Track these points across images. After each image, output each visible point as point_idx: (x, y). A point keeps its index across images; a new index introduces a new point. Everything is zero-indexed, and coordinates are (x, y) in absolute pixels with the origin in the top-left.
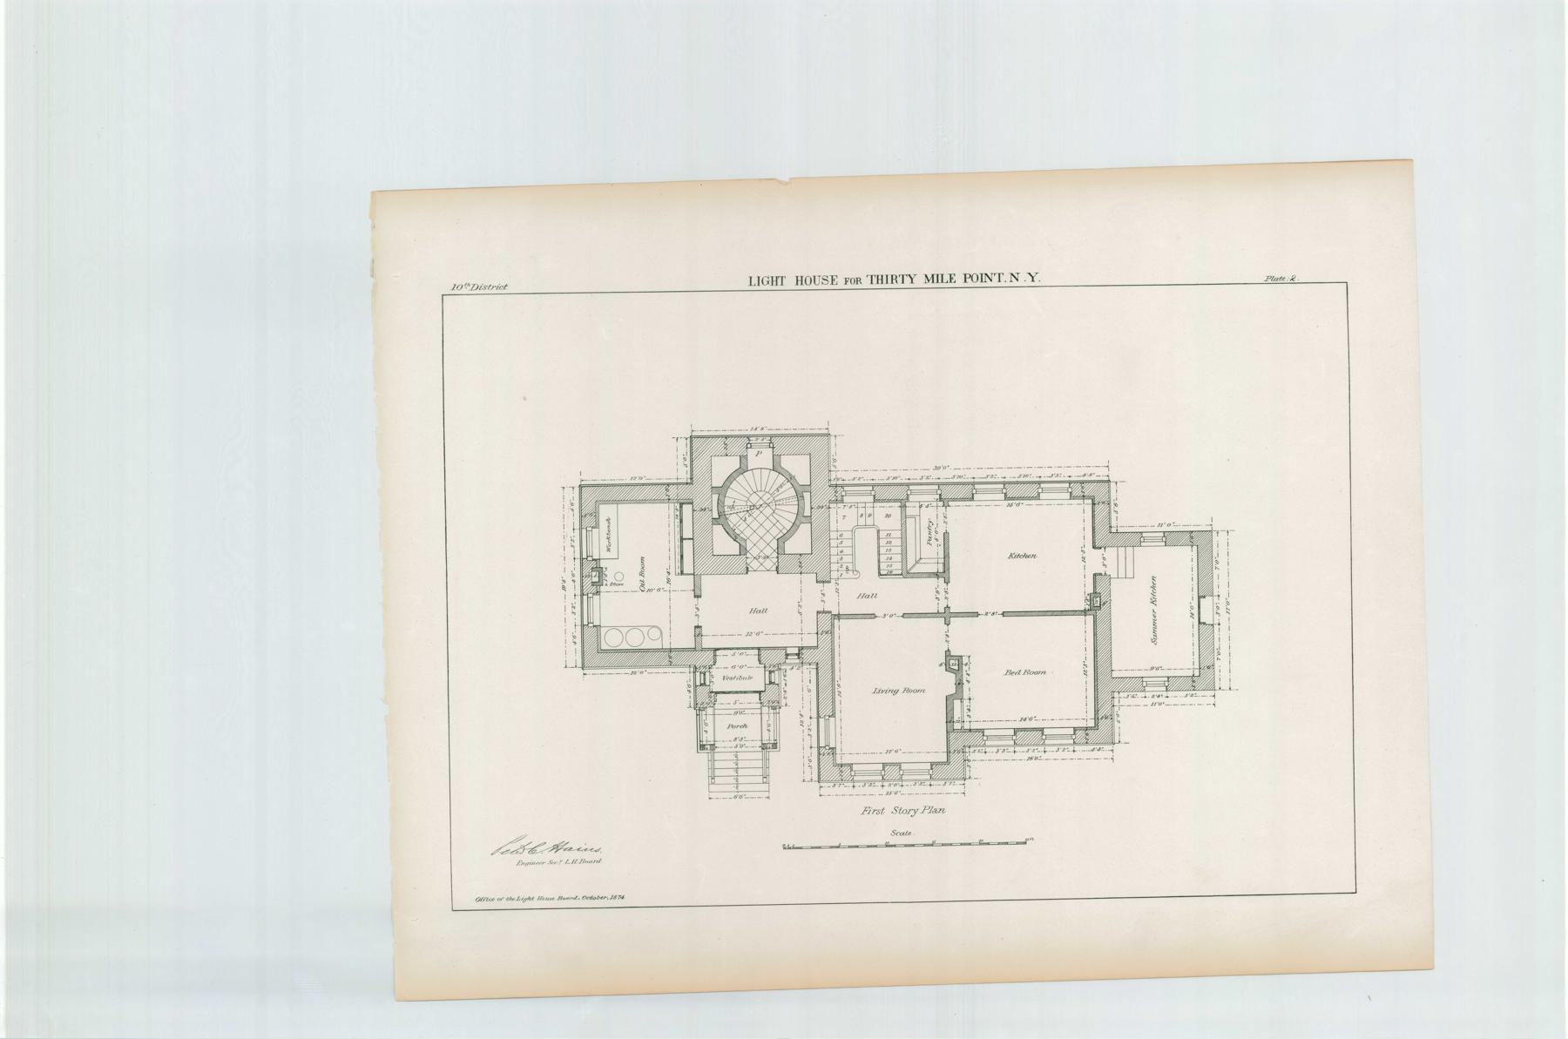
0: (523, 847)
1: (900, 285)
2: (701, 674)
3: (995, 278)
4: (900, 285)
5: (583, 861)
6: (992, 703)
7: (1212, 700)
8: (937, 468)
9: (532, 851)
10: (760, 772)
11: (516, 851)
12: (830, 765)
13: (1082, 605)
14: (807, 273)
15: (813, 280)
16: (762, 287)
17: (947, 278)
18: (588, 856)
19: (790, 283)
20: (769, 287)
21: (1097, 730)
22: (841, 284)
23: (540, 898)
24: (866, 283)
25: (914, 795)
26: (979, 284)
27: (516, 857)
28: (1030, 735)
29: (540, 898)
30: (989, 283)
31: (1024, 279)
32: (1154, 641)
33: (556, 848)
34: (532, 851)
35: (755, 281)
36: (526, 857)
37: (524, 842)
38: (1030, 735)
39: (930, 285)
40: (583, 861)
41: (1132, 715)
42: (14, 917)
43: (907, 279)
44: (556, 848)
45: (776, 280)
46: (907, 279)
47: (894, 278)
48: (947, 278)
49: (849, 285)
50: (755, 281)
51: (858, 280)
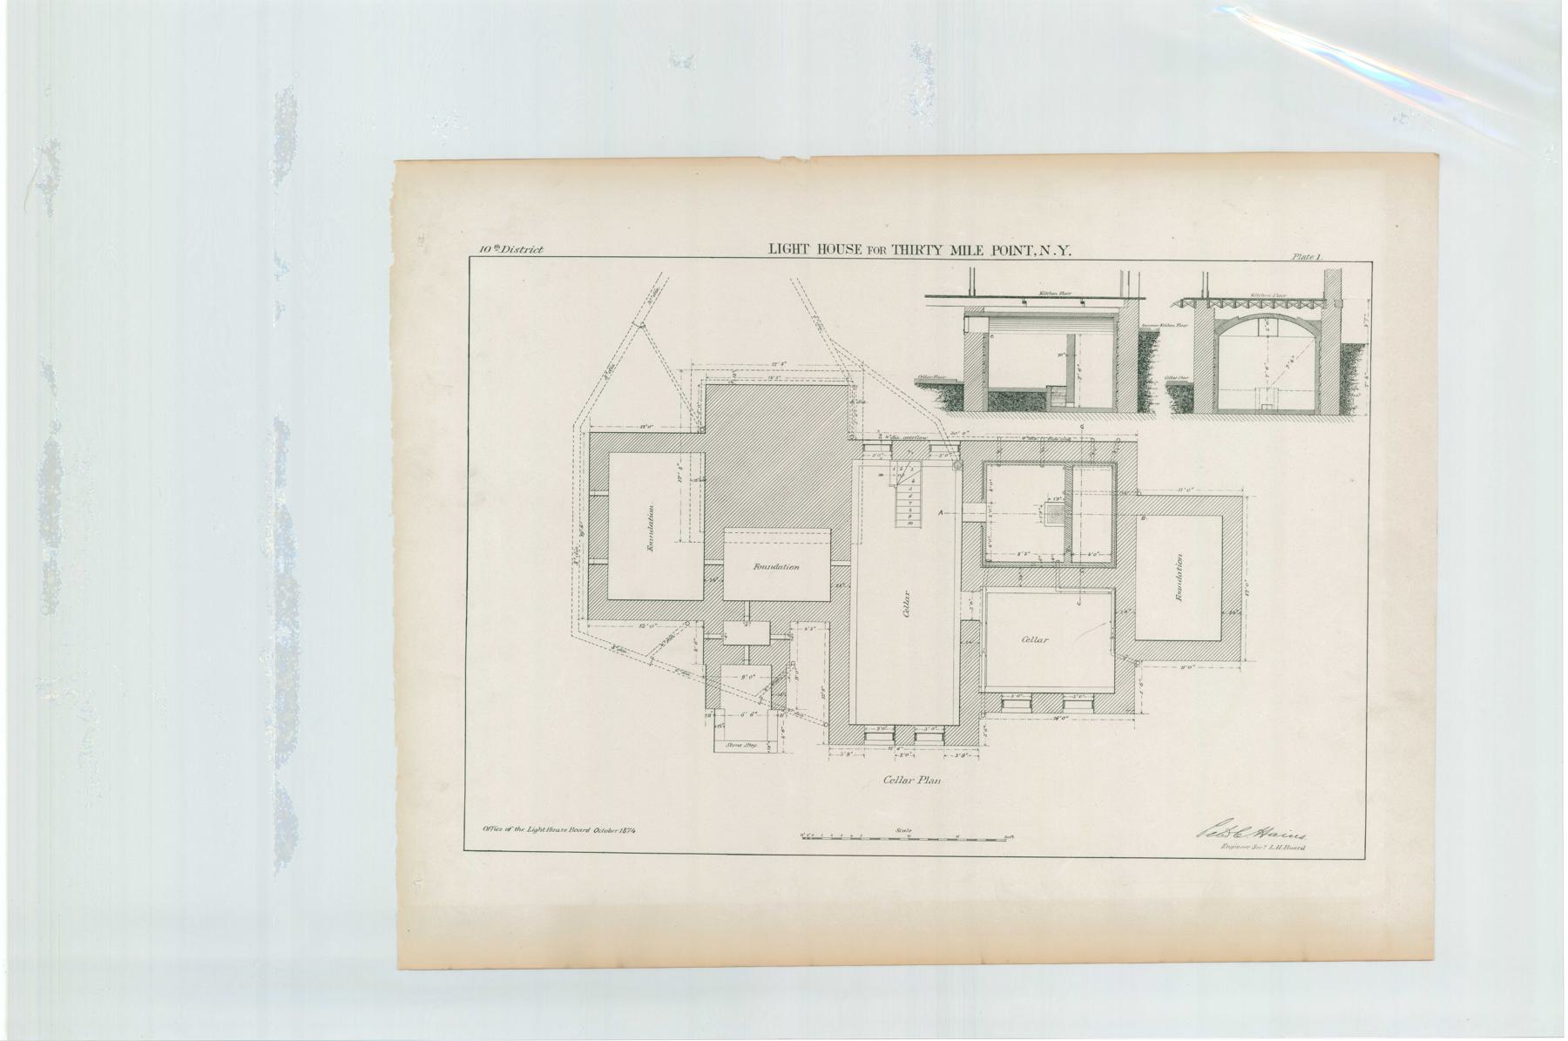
0: (1229, 831)
2: (711, 639)
3: (1025, 251)
6: (1007, 667)
9: (1237, 835)
11: (1221, 834)
12: (846, 732)
14: (831, 241)
15: (837, 248)
17: (974, 250)
18: (1294, 842)
21: (1115, 701)
22: (865, 254)
24: (890, 252)
25: (927, 758)
26: (836, 255)
27: (1222, 840)
28: (1047, 702)
30: (1018, 256)
33: (1261, 833)
34: (1237, 835)
35: (775, 248)
36: (1231, 840)
37: (1230, 825)
38: (1047, 702)
41: (1156, 678)
43: (933, 251)
44: (1261, 833)
46: (933, 251)
47: (919, 250)
48: (974, 250)
49: (873, 255)
50: (775, 248)
51: (880, 250)
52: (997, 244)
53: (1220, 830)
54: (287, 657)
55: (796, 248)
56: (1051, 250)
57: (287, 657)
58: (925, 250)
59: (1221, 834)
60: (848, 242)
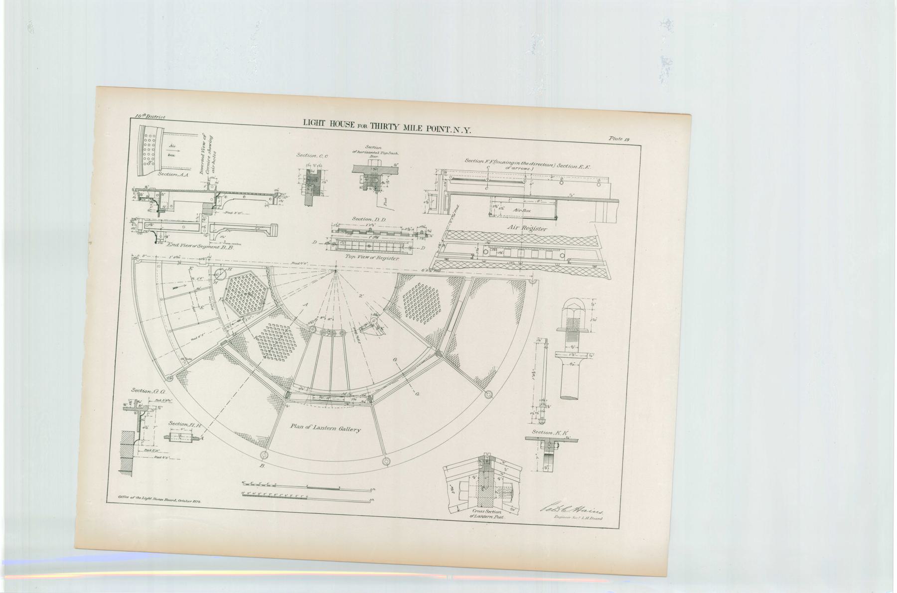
0: (559, 508)
1: (389, 130)
3: (445, 129)
9: (564, 510)
10: (327, 340)
13: (517, 293)
14: (337, 119)
16: (311, 126)
17: (417, 128)
19: (327, 124)
24: (369, 128)
26: (436, 133)
30: (442, 133)
33: (577, 510)
34: (564, 510)
35: (307, 122)
36: (560, 513)
37: (559, 505)
39: (406, 131)
42: (9, 523)
43: (393, 127)
44: (577, 510)
45: (321, 122)
46: (393, 127)
47: (385, 126)
49: (360, 129)
50: (307, 122)
51: (365, 126)
53: (553, 507)
56: (460, 130)
58: (389, 127)
60: (349, 120)
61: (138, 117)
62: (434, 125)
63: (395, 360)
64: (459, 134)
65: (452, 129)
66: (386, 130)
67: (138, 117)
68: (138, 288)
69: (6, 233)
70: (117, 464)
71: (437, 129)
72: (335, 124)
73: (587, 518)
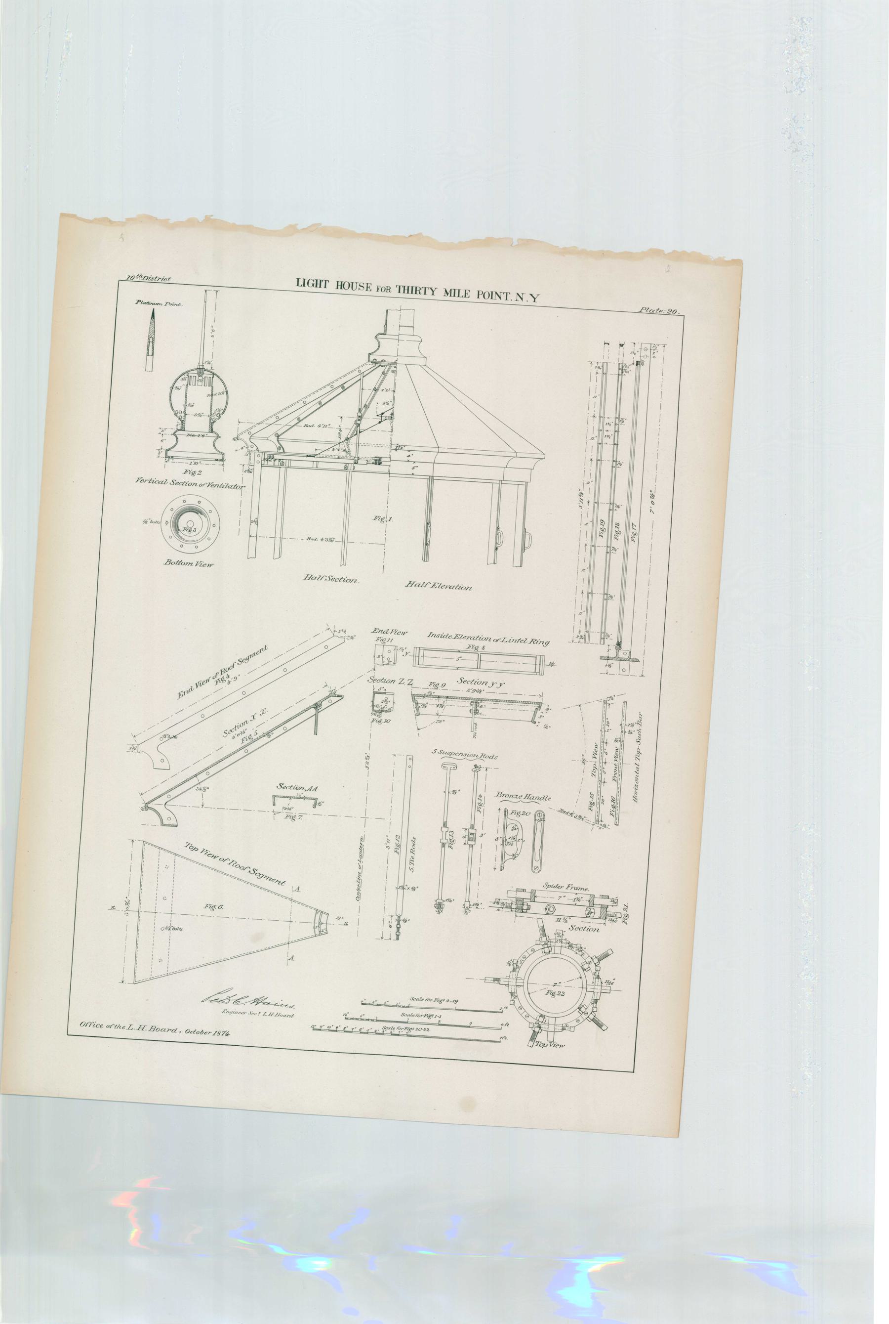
0: (229, 999)
3: (503, 296)
4: (422, 296)
5: (278, 1015)
7: (386, 936)
8: (584, 761)
9: (236, 1002)
11: (223, 1001)
14: (346, 278)
15: (351, 285)
16: (306, 288)
17: (462, 293)
18: (284, 1011)
20: (314, 289)
23: (428, 1000)
24: (395, 290)
26: (489, 300)
29: (428, 1000)
31: (527, 298)
32: (310, 577)
33: (257, 1001)
35: (301, 282)
36: (231, 1006)
37: (230, 994)
39: (448, 298)
40: (278, 1015)
43: (429, 292)
44: (257, 1001)
46: (429, 292)
47: (415, 290)
48: (462, 293)
50: (301, 282)
51: (388, 289)
52: (319, 278)
53: (221, 997)
54: (660, 312)
55: (318, 283)
57: (660, 312)
58: (422, 291)
59: (223, 1001)
61: (131, 279)
62: (487, 289)
63: (622, 345)
64: (524, 302)
65: (513, 297)
66: (418, 296)
67: (131, 279)
68: (307, 936)
69: (873, 1241)
70: (385, 294)
71: (491, 295)
72: (342, 286)
73: (271, 1015)
